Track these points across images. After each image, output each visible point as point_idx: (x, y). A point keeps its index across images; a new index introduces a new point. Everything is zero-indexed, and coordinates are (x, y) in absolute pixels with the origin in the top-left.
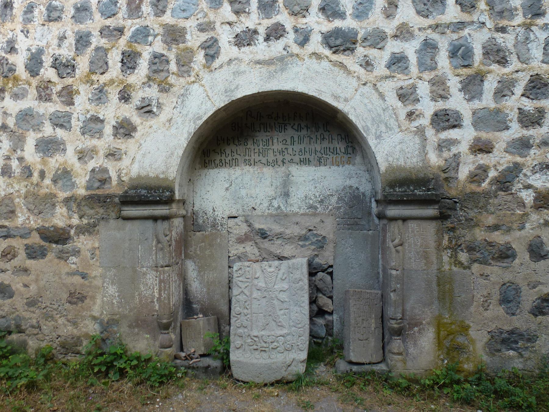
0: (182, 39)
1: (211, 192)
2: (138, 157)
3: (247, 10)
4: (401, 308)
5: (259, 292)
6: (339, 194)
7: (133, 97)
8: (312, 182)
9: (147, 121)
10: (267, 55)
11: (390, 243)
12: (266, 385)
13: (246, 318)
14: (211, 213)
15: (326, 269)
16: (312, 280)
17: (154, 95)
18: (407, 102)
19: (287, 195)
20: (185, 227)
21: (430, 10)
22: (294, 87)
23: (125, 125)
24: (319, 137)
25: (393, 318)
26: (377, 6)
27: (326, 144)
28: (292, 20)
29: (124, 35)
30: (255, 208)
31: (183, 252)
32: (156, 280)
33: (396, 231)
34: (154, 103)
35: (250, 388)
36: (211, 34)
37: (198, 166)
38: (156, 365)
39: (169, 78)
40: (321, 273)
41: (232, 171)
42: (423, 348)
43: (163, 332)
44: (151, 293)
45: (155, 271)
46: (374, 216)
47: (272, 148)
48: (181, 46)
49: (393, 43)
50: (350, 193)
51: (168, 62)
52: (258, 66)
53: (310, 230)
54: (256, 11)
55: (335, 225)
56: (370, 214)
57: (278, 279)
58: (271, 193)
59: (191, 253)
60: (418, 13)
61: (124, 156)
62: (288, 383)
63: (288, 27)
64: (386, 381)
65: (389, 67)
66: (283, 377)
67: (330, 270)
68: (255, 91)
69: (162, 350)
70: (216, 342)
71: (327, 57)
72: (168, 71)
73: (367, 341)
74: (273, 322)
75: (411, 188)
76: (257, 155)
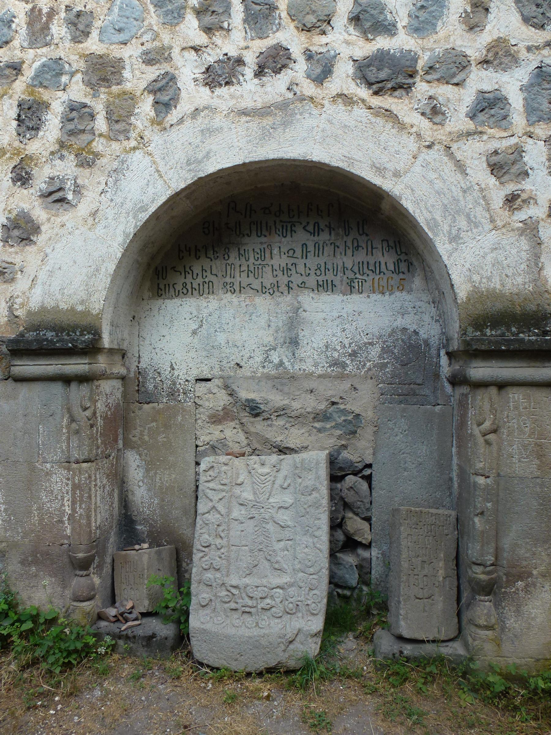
0: (117, 77)
1: (168, 338)
2: (42, 276)
3: (225, 25)
4: (493, 545)
5: (242, 507)
6: (384, 342)
7: (36, 176)
8: (338, 321)
9: (57, 216)
10: (260, 100)
11: (475, 427)
12: (249, 675)
13: (219, 553)
14: (167, 372)
15: (361, 471)
16: (337, 488)
17: (69, 172)
18: (506, 177)
19: (294, 342)
20: (125, 395)
21: (547, 15)
22: (306, 153)
23: (22, 223)
24: (349, 244)
25: (479, 562)
26: (452, 11)
27: (361, 256)
28: (303, 39)
29: (23, 75)
30: (242, 364)
31: (121, 437)
32: (67, 484)
33: (487, 406)
34: (69, 185)
35: (220, 680)
36: (165, 67)
37: (147, 294)
38: (62, 632)
39: (94, 144)
40: (351, 476)
41: (202, 302)
42: (533, 619)
43: (78, 572)
44: (58, 506)
45: (65, 468)
46: (445, 380)
47: (270, 264)
48: (115, 89)
49: (480, 73)
50: (403, 340)
51: (92, 117)
52: (244, 119)
53: (333, 403)
54: (241, 27)
55: (375, 395)
56: (437, 376)
57: (276, 486)
58: (268, 339)
59: (134, 439)
60: (526, 20)
61: (19, 276)
62: (289, 672)
63: (296, 51)
64: (464, 676)
65: (472, 117)
66: (279, 663)
67: (367, 472)
68: (237, 160)
69: (75, 604)
70: (169, 592)
71: (363, 101)
72: (92, 131)
73: (430, 601)
74: (265, 562)
75: (514, 329)
76: (244, 275)
